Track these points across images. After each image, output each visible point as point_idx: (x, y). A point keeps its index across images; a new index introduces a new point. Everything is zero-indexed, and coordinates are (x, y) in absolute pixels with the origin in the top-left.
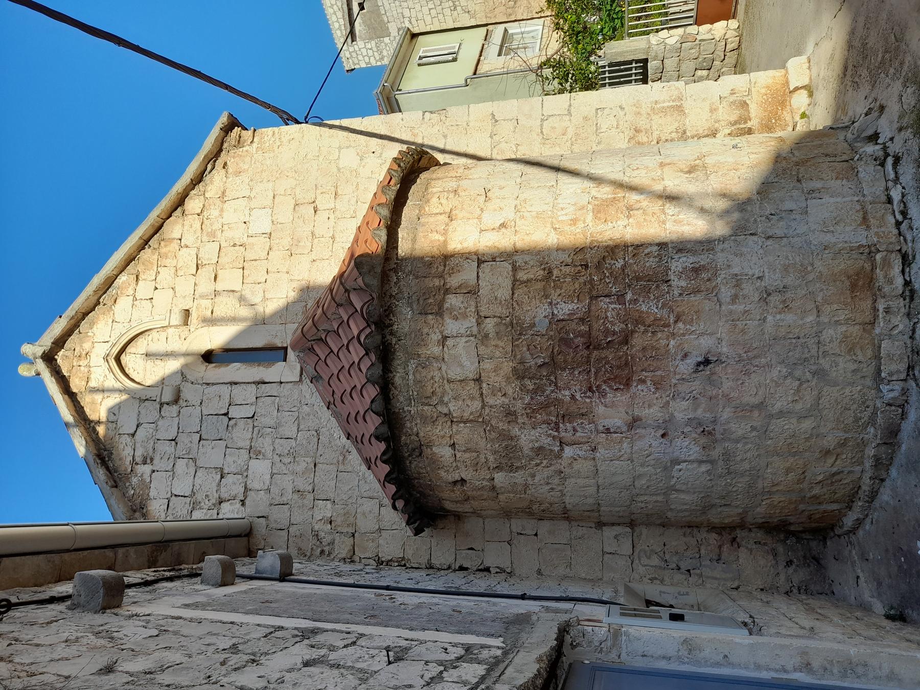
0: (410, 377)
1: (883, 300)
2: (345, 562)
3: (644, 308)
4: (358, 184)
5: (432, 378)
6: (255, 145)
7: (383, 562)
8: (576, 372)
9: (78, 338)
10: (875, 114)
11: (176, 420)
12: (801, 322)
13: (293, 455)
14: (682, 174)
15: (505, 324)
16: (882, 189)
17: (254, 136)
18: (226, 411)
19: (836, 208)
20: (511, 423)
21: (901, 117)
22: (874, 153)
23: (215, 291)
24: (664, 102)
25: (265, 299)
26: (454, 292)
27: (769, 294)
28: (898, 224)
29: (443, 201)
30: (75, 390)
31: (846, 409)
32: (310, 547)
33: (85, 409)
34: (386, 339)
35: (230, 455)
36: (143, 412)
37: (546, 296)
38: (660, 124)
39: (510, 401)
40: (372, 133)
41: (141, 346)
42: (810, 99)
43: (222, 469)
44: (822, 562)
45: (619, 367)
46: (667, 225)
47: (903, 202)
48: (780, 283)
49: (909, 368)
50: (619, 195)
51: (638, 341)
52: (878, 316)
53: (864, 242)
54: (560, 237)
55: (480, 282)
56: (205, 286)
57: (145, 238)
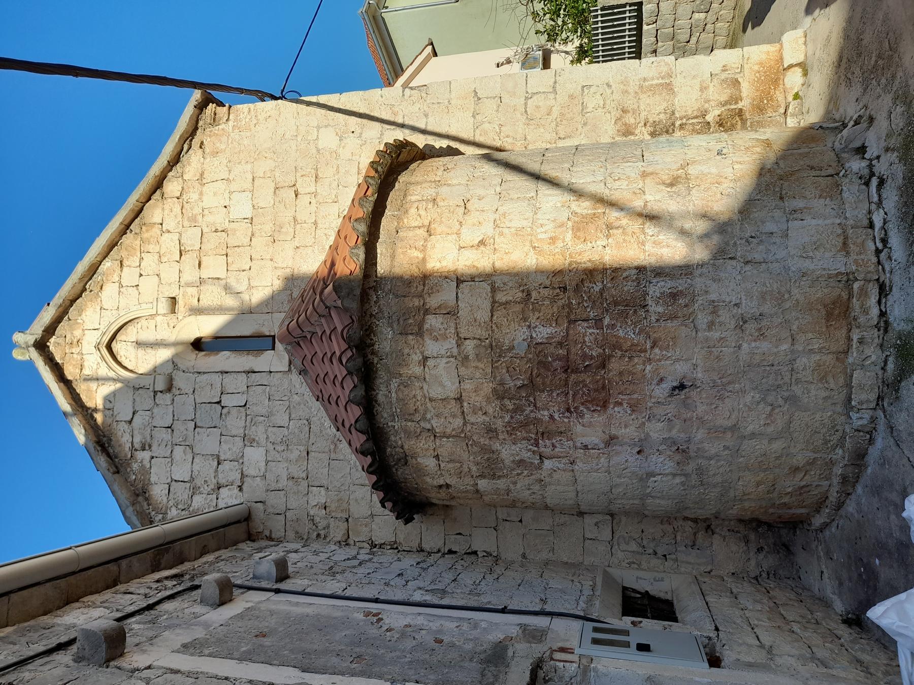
0: (393, 395)
1: (857, 331)
2: (340, 544)
3: (621, 333)
4: (338, 167)
5: (414, 396)
6: (231, 123)
7: (376, 545)
8: (555, 394)
9: (68, 325)
10: (864, 125)
11: (171, 408)
12: (775, 350)
13: (286, 443)
14: (664, 188)
15: (485, 346)
16: (864, 212)
17: (229, 114)
18: (219, 400)
19: (817, 232)
20: (492, 439)
21: (888, 136)
22: (860, 170)
23: (200, 278)
24: (653, 79)
25: (250, 287)
26: (434, 312)
27: (745, 322)
28: (878, 252)
29: (422, 212)
30: (69, 378)
31: (816, 432)
32: (306, 530)
33: (81, 396)
34: (367, 358)
35: (225, 442)
36: (137, 399)
37: (525, 319)
38: (648, 104)
39: (491, 419)
40: (351, 111)
41: (130, 334)
42: (805, 78)
43: (218, 456)
44: (791, 548)
45: (596, 390)
46: (647, 247)
47: (885, 229)
48: (757, 311)
49: (878, 398)
50: (599, 211)
51: (615, 365)
52: (852, 345)
53: (843, 270)
54: (539, 257)
55: (459, 302)
56: (191, 274)
57: (126, 222)
